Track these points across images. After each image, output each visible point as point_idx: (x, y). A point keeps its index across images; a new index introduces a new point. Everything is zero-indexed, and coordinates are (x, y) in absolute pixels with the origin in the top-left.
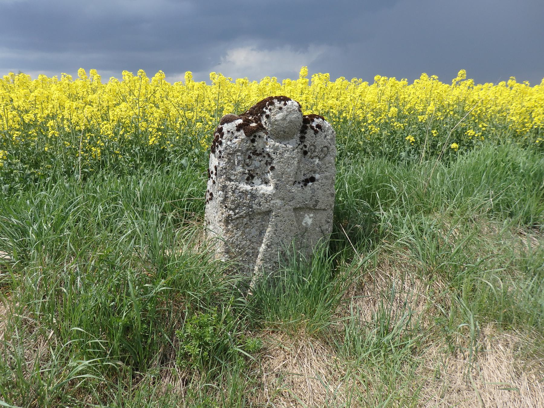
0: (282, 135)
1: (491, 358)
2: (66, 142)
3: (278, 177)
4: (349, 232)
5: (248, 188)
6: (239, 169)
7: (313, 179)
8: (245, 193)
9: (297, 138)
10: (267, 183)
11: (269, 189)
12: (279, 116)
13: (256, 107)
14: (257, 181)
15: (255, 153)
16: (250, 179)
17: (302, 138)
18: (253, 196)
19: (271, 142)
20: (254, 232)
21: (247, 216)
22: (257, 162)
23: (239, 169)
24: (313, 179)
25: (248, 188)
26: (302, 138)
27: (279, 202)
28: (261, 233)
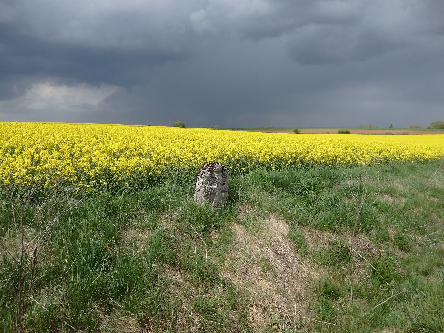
0: (218, 173)
1: (272, 218)
2: (89, 186)
3: (217, 183)
4: (232, 196)
5: (211, 187)
6: (209, 182)
7: (224, 184)
8: (210, 188)
9: (221, 173)
10: (214, 185)
11: (215, 187)
12: (218, 168)
13: (319, 164)
14: (212, 185)
15: (212, 177)
16: (211, 185)
17: (222, 173)
18: (212, 189)
19: (216, 174)
20: (211, 199)
21: (210, 194)
22: (213, 180)
23: (209, 182)
24: (224, 184)
25: (211, 187)
26: (222, 173)
27: (217, 190)
28: (213, 199)
